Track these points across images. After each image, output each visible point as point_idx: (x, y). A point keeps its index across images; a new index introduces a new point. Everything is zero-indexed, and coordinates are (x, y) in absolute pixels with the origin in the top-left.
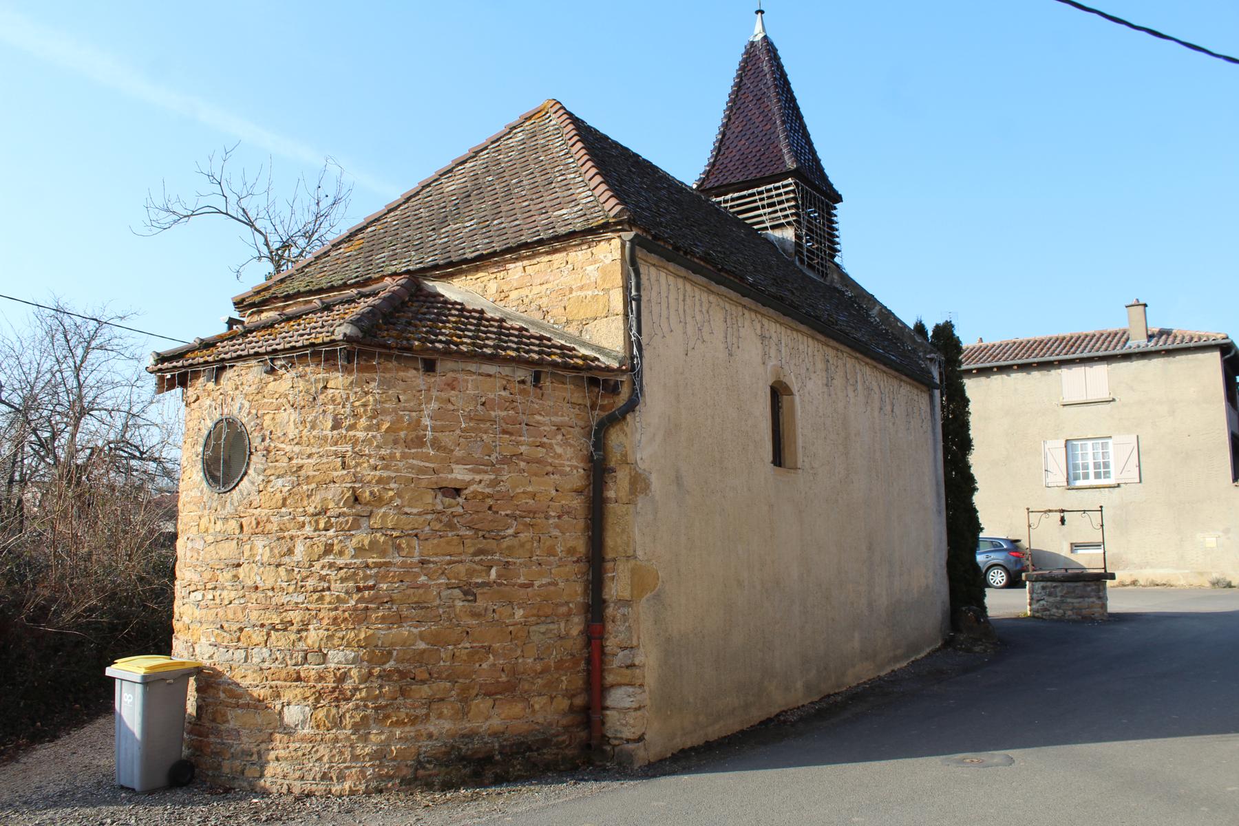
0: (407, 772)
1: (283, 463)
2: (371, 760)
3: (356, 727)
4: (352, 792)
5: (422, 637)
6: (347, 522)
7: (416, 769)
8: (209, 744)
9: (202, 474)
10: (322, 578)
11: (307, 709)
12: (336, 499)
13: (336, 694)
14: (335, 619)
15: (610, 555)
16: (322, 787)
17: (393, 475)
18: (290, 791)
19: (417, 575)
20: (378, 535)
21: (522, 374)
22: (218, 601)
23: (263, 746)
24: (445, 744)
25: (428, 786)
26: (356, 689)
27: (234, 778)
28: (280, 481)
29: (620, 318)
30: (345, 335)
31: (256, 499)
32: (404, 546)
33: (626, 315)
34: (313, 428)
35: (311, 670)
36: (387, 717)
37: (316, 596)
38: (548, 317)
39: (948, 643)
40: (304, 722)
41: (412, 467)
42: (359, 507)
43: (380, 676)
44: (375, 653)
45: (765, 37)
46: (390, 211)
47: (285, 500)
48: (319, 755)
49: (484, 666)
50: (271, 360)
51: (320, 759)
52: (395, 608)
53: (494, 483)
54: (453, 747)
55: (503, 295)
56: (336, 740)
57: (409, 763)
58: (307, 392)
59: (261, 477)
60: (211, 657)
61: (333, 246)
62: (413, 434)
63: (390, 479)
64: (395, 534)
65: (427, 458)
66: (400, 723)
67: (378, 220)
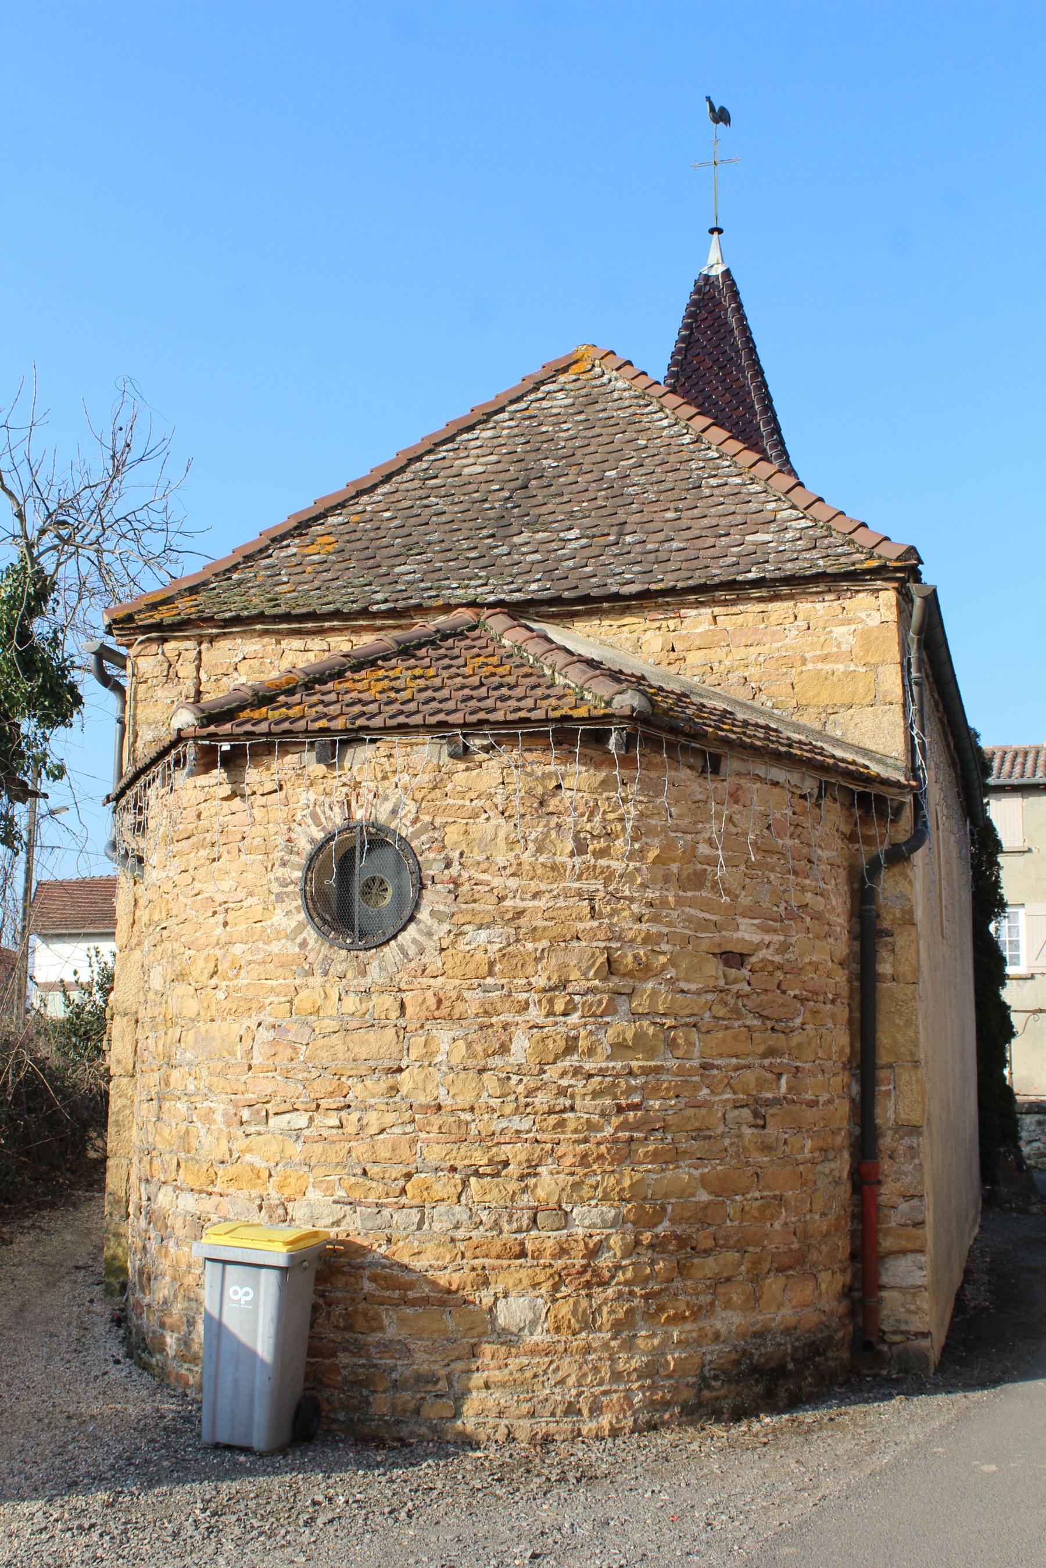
0: (688, 1395)
1: (487, 906)
2: (639, 1378)
3: (617, 1327)
4: (615, 1433)
5: (704, 1182)
6: (600, 1002)
7: (700, 1390)
8: (335, 1369)
9: (302, 916)
10: (562, 1092)
11: (540, 1301)
12: (584, 966)
13: (587, 1276)
14: (585, 1156)
15: (884, 1058)
16: (566, 1426)
17: (665, 930)
18: (510, 1438)
19: (696, 1088)
20: (645, 1023)
21: (809, 785)
22: (351, 1129)
23: (459, 1366)
24: (735, 1348)
25: (717, 1415)
26: (618, 1267)
27: (398, 1422)
28: (483, 935)
29: (898, 708)
30: (633, 709)
31: (434, 961)
32: (680, 1041)
33: (904, 705)
34: (540, 850)
35: (544, 1239)
36: (661, 1309)
37: (553, 1119)
38: (762, 697)
39: (989, 1201)
40: (534, 1323)
41: (689, 919)
42: (615, 979)
43: (651, 1246)
44: (644, 1210)
45: (727, 273)
46: (360, 494)
47: (491, 964)
48: (560, 1374)
49: (777, 1225)
50: (463, 734)
51: (561, 1382)
52: (669, 1140)
53: (784, 948)
54: (744, 1351)
55: (673, 656)
56: (588, 1350)
57: (692, 1380)
58: (529, 792)
59: (446, 927)
60: (337, 1223)
61: (274, 540)
62: (689, 869)
63: (660, 935)
64: (669, 1022)
65: (705, 906)
66: (677, 1319)
67: (342, 505)
